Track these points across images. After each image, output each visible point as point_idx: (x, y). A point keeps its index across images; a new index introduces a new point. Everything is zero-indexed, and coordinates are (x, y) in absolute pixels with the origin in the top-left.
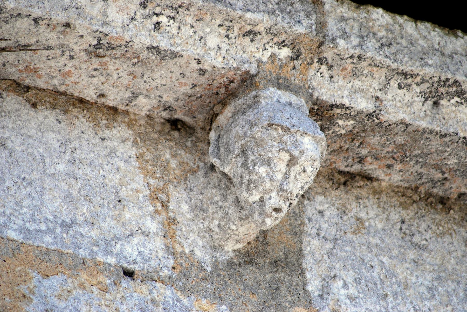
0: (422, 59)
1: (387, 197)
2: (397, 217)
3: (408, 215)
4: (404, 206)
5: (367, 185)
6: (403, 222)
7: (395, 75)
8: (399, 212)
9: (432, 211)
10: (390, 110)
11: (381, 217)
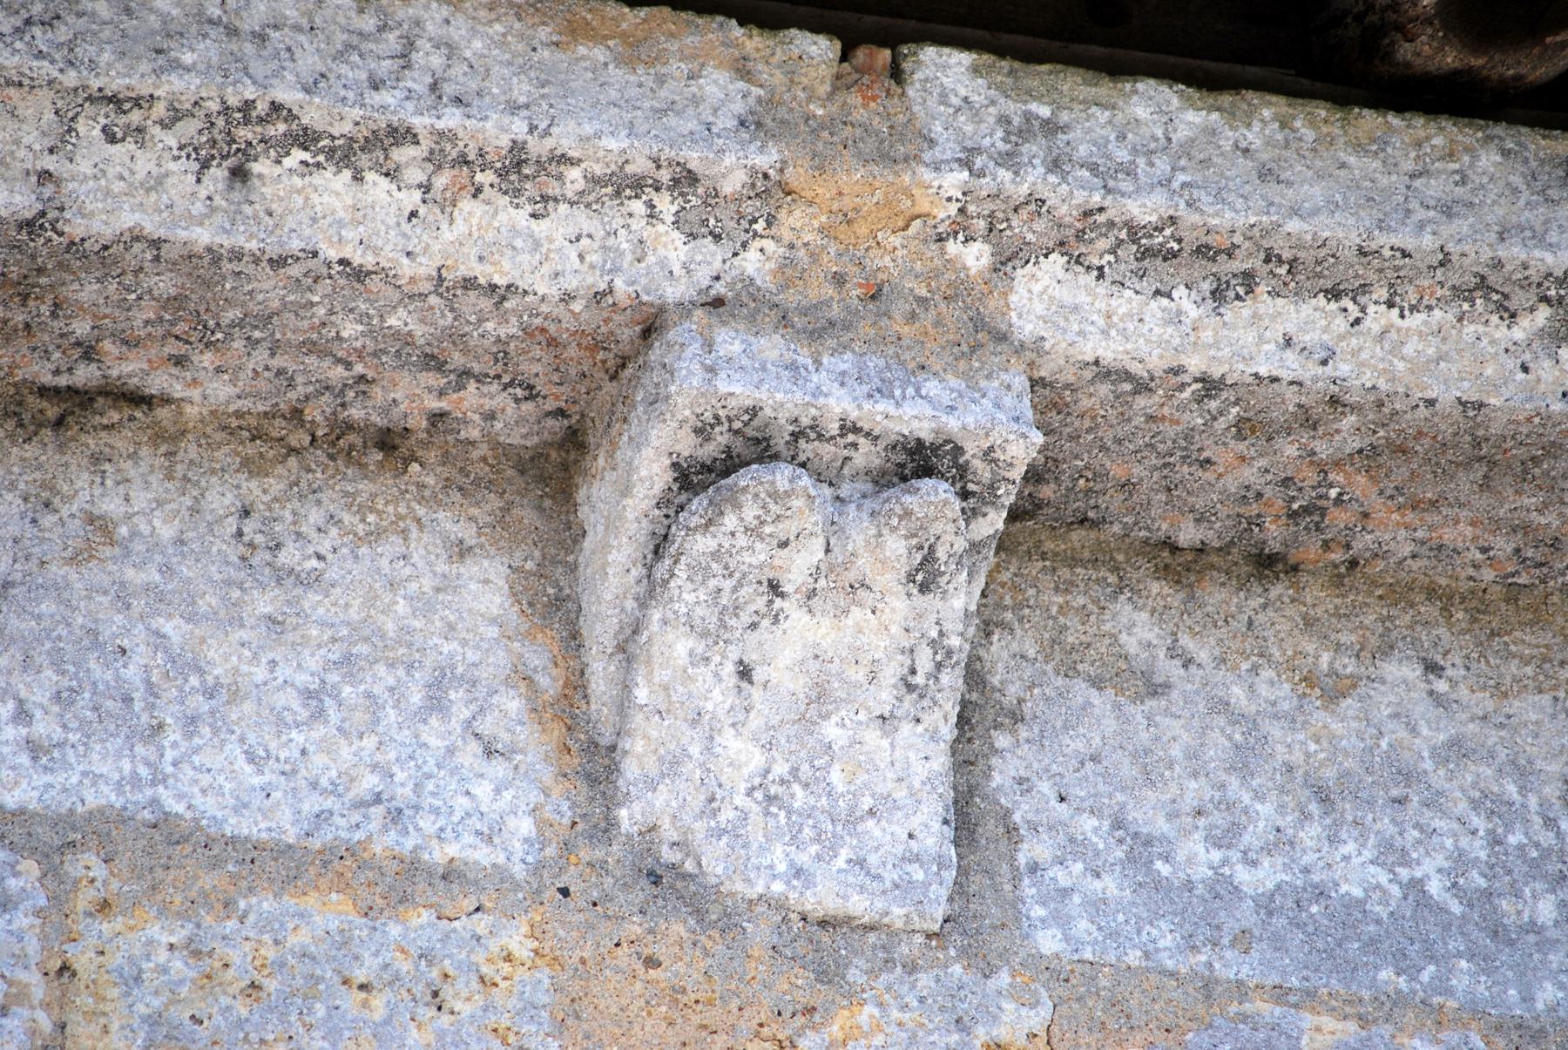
0: (159, 51)
1: (200, 446)
2: (229, 498)
3: (265, 492)
4: (252, 467)
5: (132, 419)
6: (246, 513)
7: (87, 105)
8: (238, 487)
9: (349, 471)
10: (89, 207)
11: (173, 506)
